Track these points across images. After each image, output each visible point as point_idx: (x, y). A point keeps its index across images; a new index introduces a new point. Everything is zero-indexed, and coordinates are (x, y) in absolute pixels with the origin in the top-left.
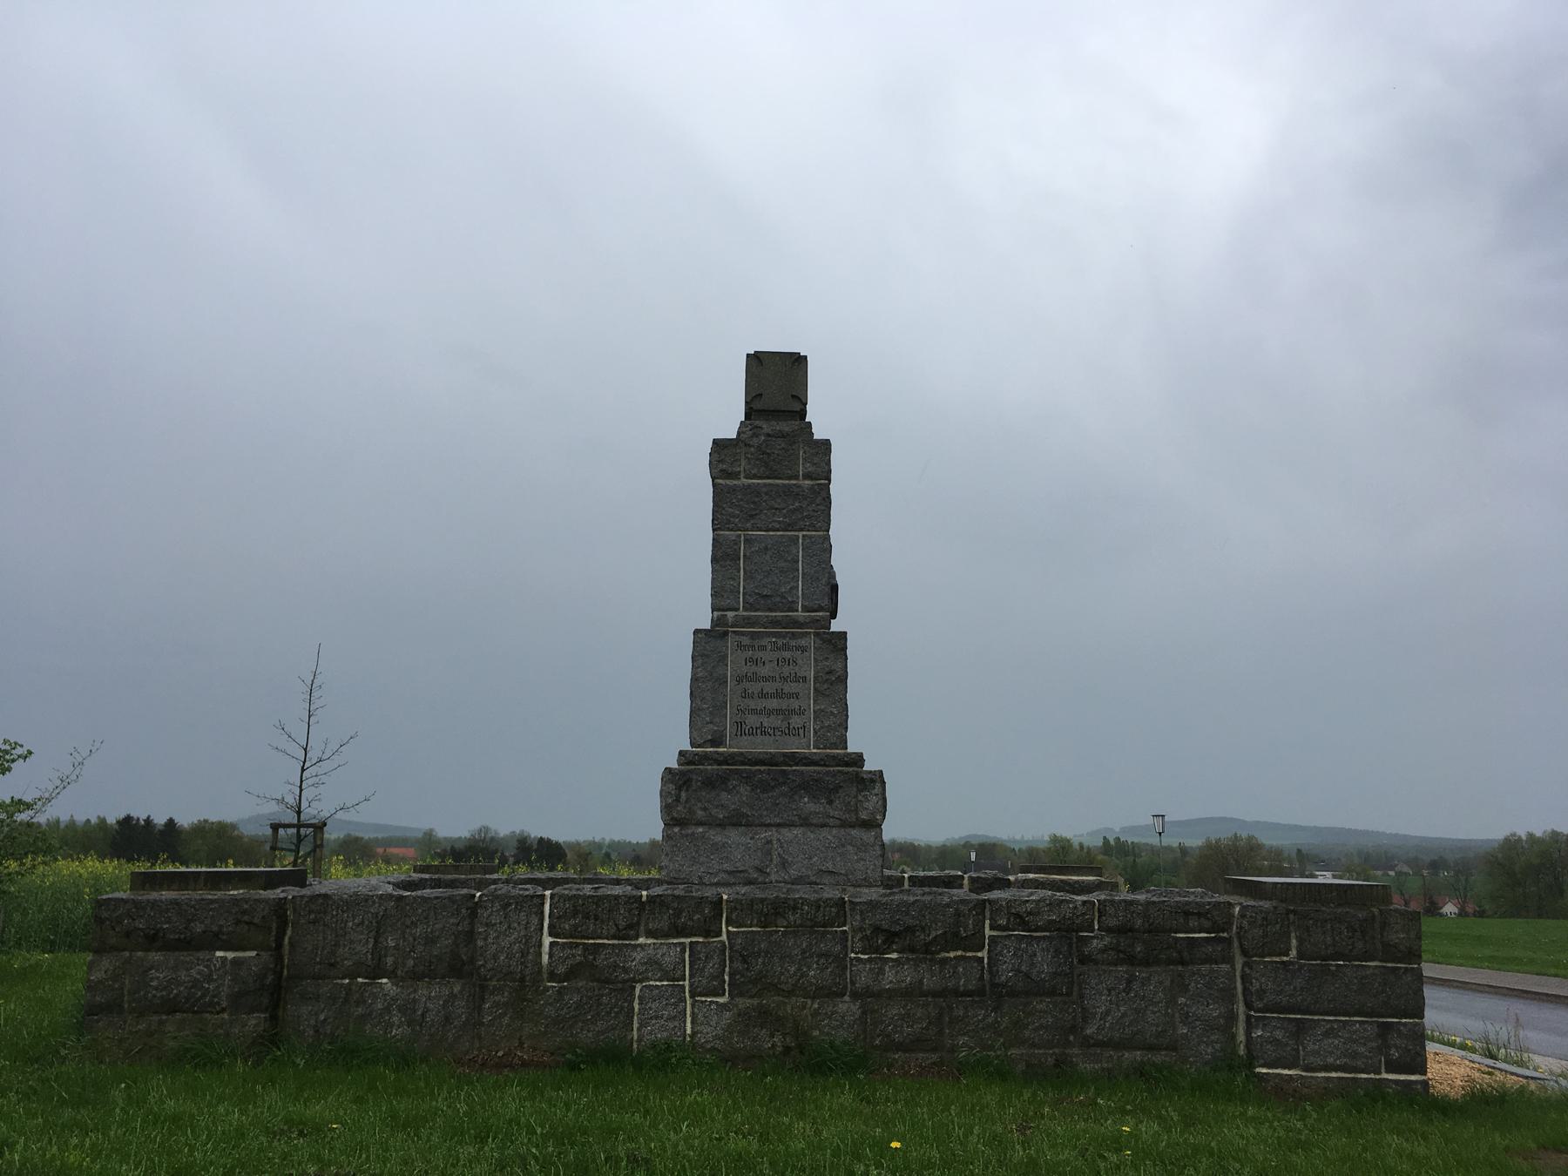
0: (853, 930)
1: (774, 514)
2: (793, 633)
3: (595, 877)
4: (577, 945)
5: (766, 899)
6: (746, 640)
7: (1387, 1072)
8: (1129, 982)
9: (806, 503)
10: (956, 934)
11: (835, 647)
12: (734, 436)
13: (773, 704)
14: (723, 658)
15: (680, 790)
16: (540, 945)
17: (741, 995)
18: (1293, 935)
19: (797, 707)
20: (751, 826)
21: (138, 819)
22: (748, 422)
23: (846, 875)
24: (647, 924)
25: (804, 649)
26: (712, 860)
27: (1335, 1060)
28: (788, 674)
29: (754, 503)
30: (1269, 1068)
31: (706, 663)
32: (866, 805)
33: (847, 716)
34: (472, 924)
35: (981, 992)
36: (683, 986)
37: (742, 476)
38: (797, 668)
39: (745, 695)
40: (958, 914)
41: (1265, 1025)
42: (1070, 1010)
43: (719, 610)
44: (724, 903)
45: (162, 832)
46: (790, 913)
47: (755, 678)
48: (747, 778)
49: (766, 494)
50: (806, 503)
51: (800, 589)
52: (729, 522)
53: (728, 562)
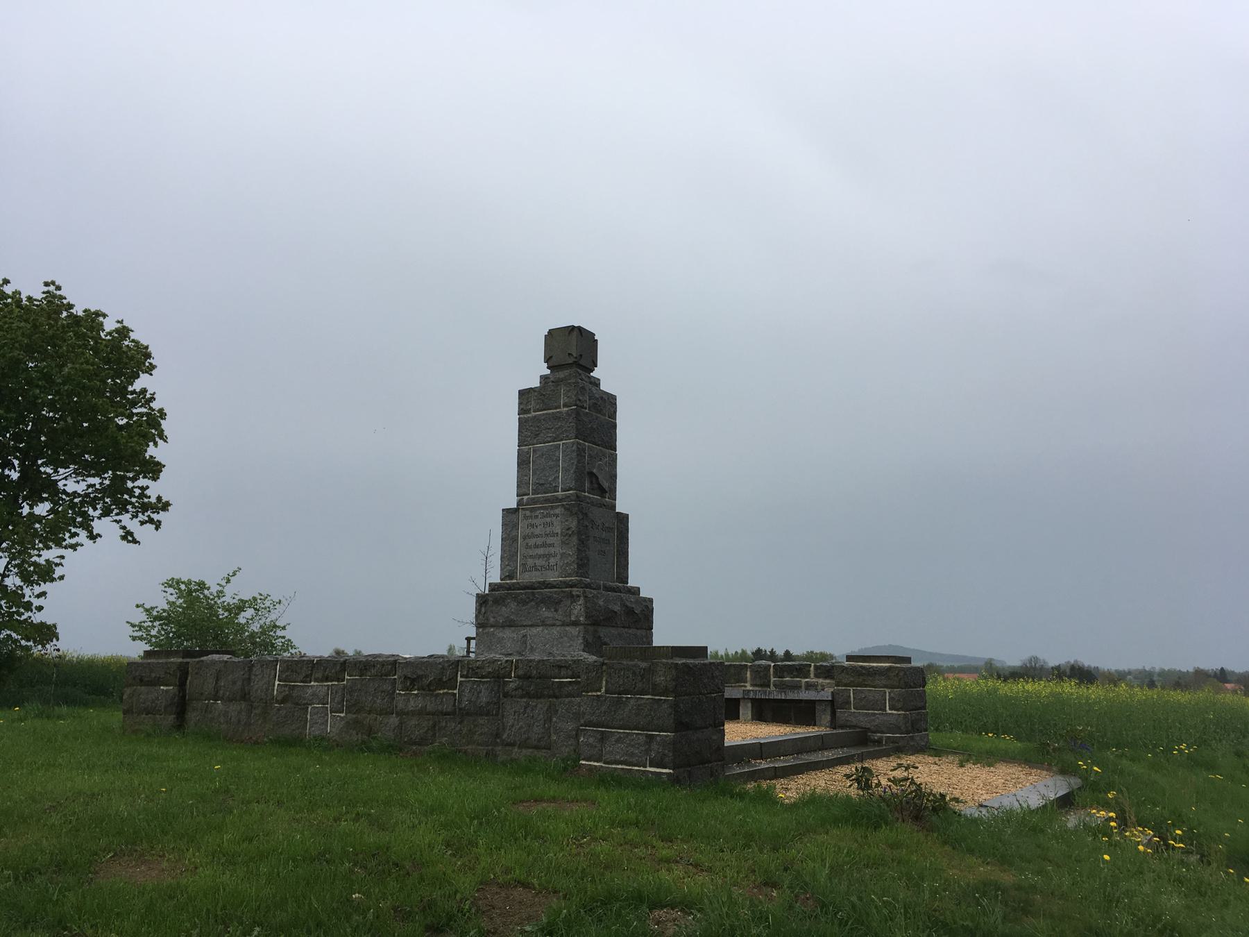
1: (548, 432)
4: (287, 685)
6: (528, 513)
7: (650, 767)
8: (526, 708)
9: (564, 422)
10: (440, 680)
11: (571, 512)
13: (541, 551)
16: (274, 686)
17: (350, 712)
18: (604, 679)
21: (766, 651)
27: (620, 758)
29: (538, 427)
30: (587, 761)
34: (250, 675)
35: (453, 713)
36: (327, 707)
40: (443, 668)
41: (585, 734)
42: (496, 724)
48: (515, 598)
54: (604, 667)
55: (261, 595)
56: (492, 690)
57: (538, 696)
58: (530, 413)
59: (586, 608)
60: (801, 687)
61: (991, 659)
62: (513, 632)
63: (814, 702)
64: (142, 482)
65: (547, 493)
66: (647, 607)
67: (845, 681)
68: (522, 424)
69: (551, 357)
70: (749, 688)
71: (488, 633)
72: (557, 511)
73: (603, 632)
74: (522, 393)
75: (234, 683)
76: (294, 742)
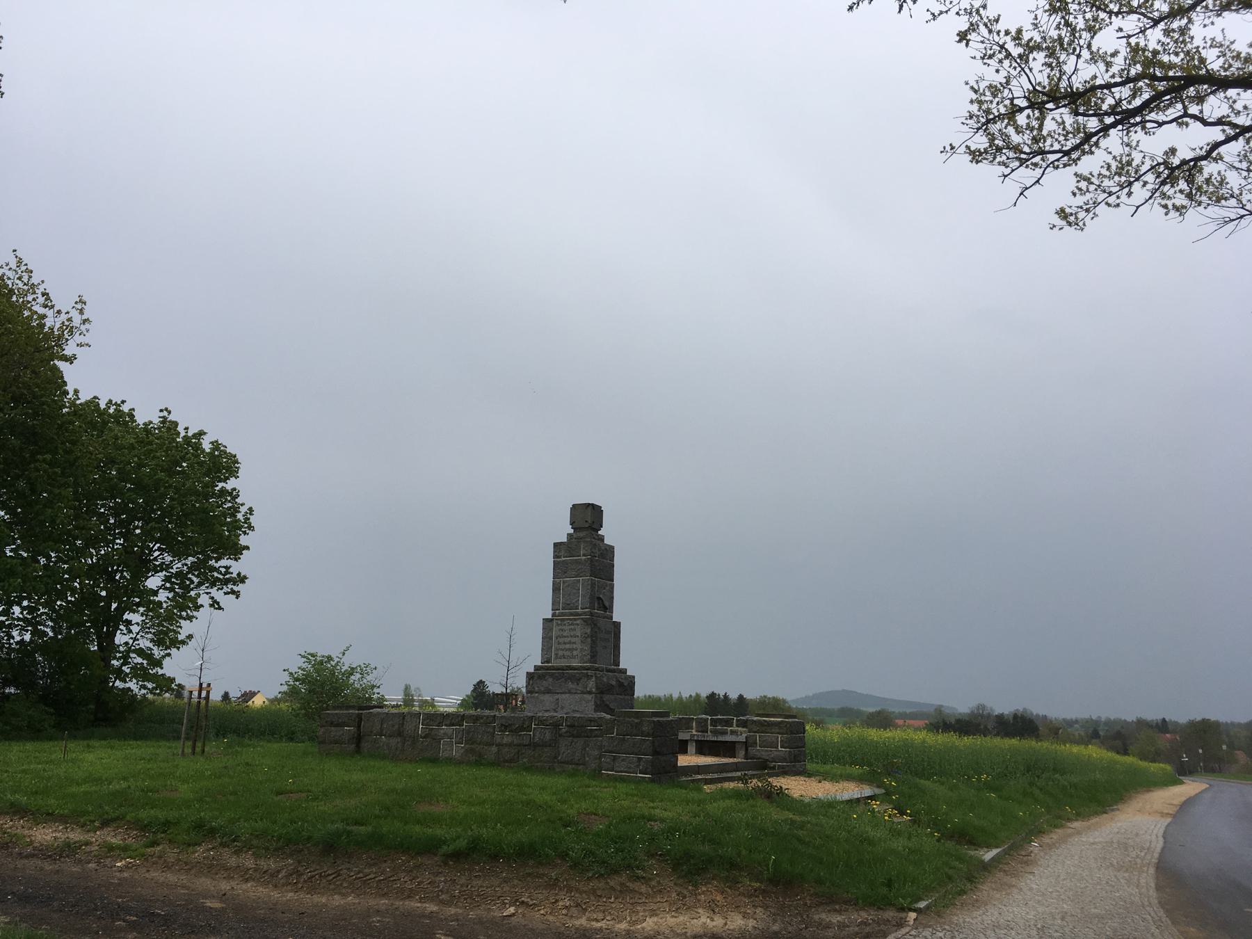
6: (559, 622)
13: (567, 646)
21: (719, 695)
35: (529, 745)
48: (552, 675)
54: (616, 722)
55: (365, 664)
56: (552, 733)
57: (578, 736)
59: (596, 683)
60: (727, 733)
61: (942, 706)
63: (735, 742)
64: (224, 562)
66: (631, 681)
67: (755, 730)
69: (574, 522)
70: (694, 733)
71: (534, 697)
72: (578, 622)
73: (607, 697)
74: (556, 545)
75: (393, 726)
76: (434, 761)
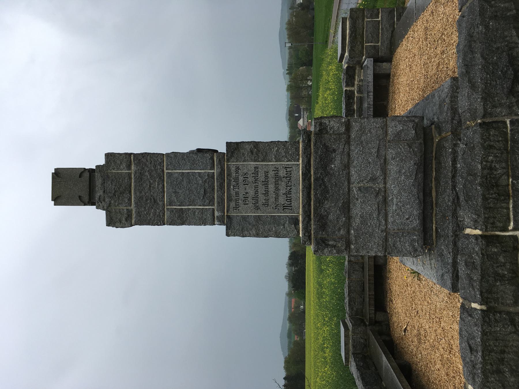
0: (509, 114)
2: (227, 176)
3: (347, 273)
5: (483, 195)
6: (233, 204)
9: (146, 168)
11: (236, 149)
12: (104, 212)
13: (271, 187)
14: (244, 218)
15: (328, 245)
19: (274, 172)
20: (349, 200)
22: (96, 203)
23: (380, 140)
24: (508, 305)
25: (238, 168)
26: (371, 224)
28: (253, 178)
29: (147, 200)
31: (247, 229)
32: (336, 128)
33: (278, 142)
37: (129, 208)
38: (250, 173)
39: (266, 204)
40: (495, 17)
43: (214, 221)
44: (486, 233)
45: (288, 381)
46: (495, 173)
47: (256, 198)
48: (319, 203)
49: (141, 192)
50: (146, 168)
51: (200, 171)
52: (159, 216)
53: (184, 215)
58: (131, 210)
61: (286, 294)
62: (355, 205)
65: (214, 186)
67: (360, 47)
68: (142, 221)
